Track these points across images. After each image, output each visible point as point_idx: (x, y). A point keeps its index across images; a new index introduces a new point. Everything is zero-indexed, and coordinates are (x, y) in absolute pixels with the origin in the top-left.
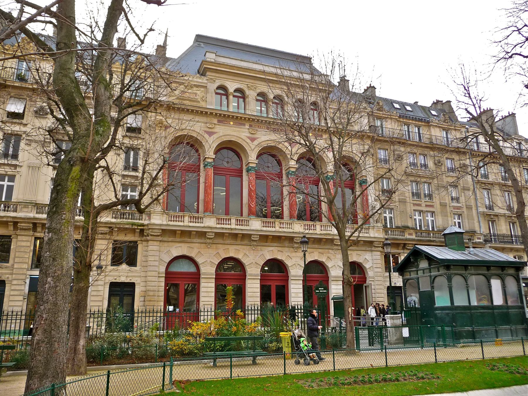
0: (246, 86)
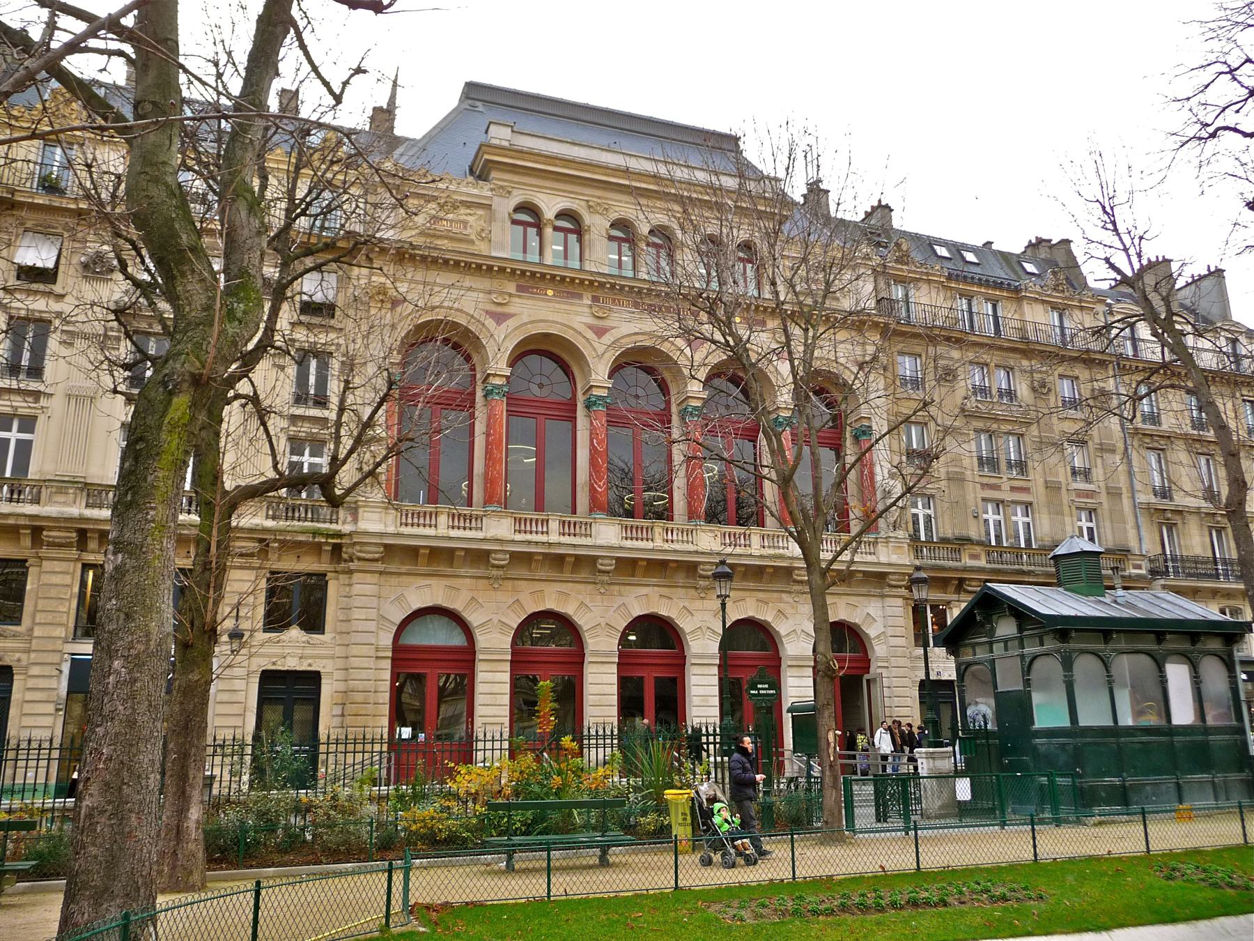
0: (583, 203)
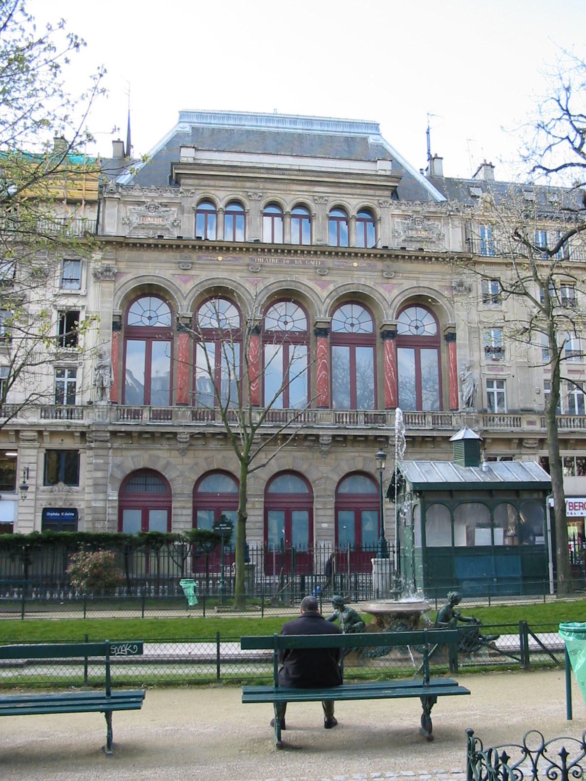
0: (244, 194)
